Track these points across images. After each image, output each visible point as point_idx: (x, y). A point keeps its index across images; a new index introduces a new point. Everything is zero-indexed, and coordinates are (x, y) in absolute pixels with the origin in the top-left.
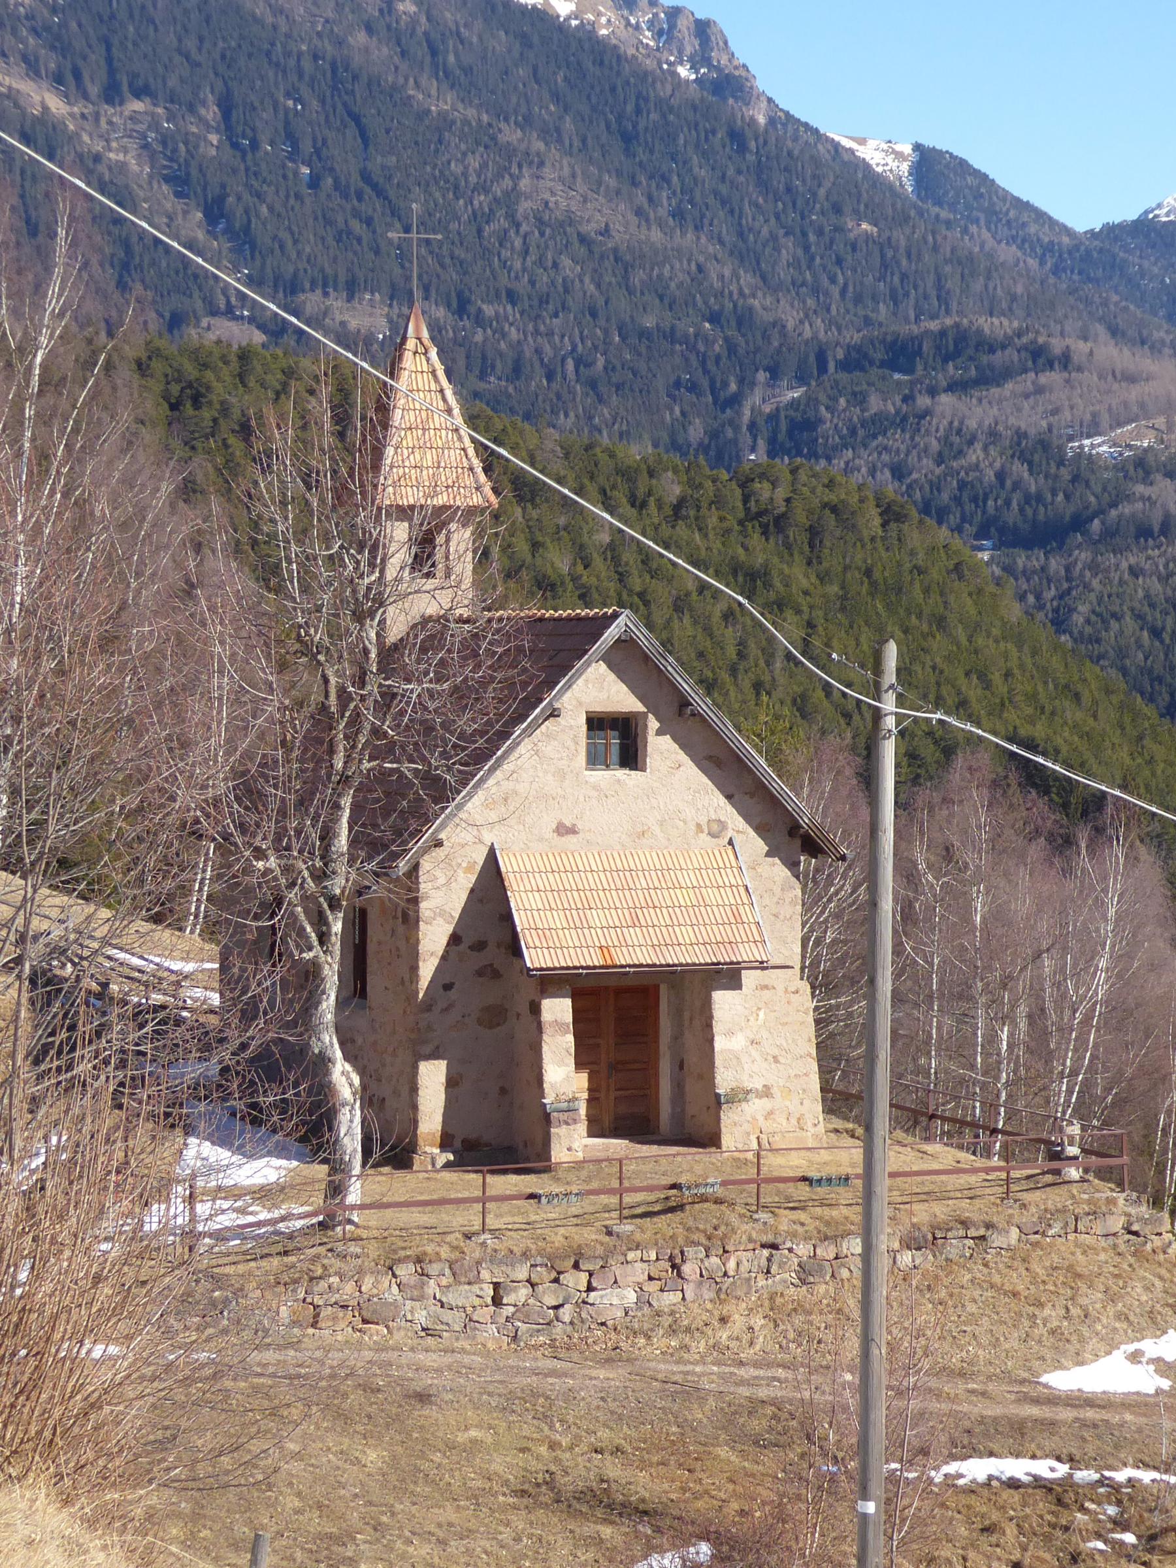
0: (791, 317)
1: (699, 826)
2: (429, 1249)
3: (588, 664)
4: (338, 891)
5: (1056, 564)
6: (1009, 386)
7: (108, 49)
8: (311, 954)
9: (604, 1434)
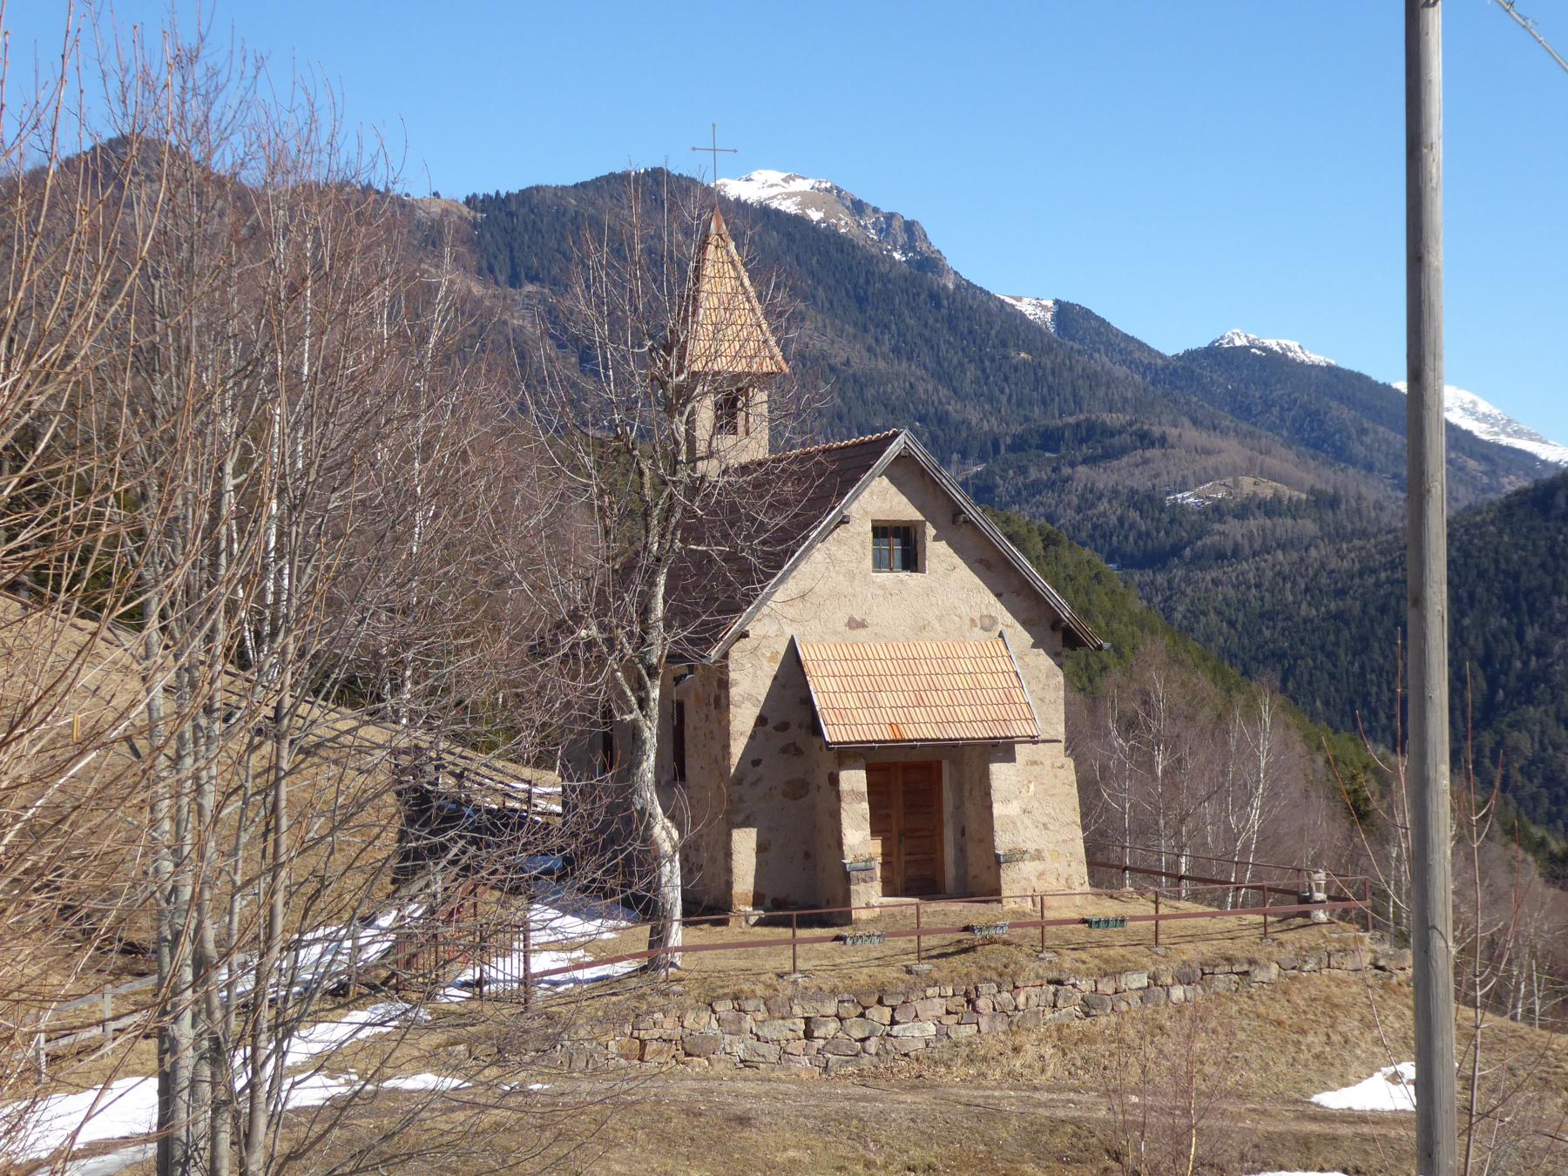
0: (974, 416)
1: (972, 621)
2: (746, 987)
3: (872, 477)
4: (655, 661)
5: (1161, 579)
6: (1125, 459)
7: (511, 251)
9: (915, 1153)
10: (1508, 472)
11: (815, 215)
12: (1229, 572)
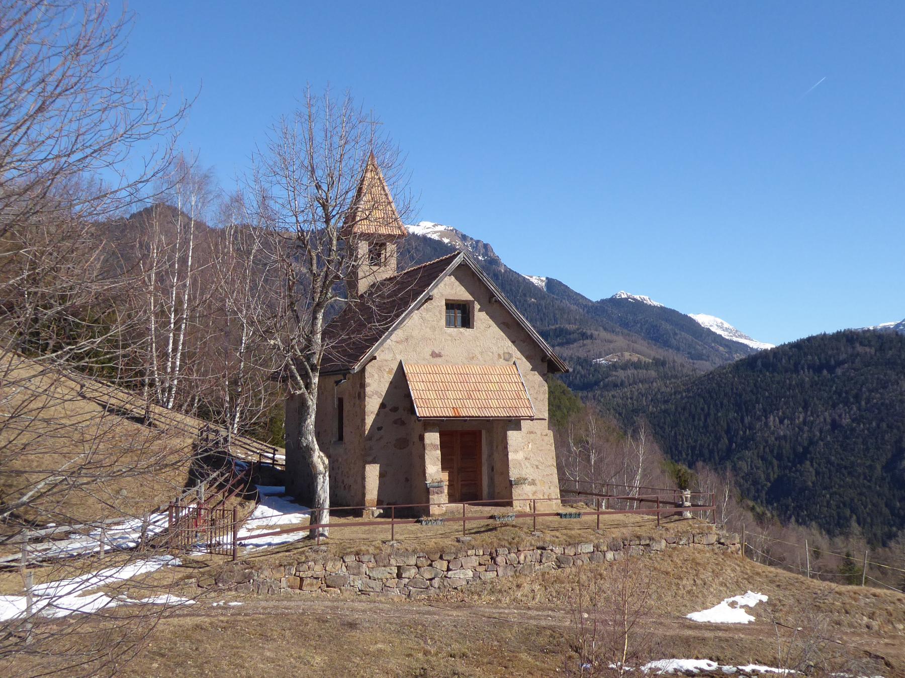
1: (499, 355)
2: (363, 548)
8: (301, 392)
9: (456, 646)
10: (736, 352)
11: (446, 241)
12: (617, 392)
